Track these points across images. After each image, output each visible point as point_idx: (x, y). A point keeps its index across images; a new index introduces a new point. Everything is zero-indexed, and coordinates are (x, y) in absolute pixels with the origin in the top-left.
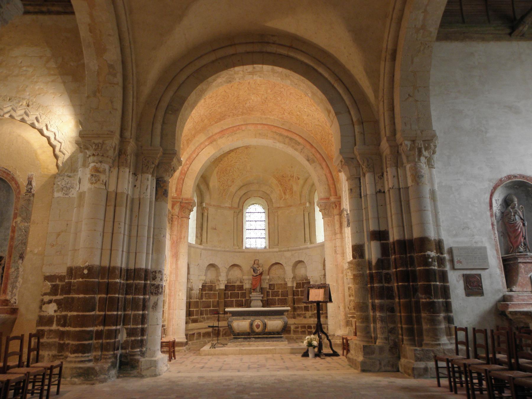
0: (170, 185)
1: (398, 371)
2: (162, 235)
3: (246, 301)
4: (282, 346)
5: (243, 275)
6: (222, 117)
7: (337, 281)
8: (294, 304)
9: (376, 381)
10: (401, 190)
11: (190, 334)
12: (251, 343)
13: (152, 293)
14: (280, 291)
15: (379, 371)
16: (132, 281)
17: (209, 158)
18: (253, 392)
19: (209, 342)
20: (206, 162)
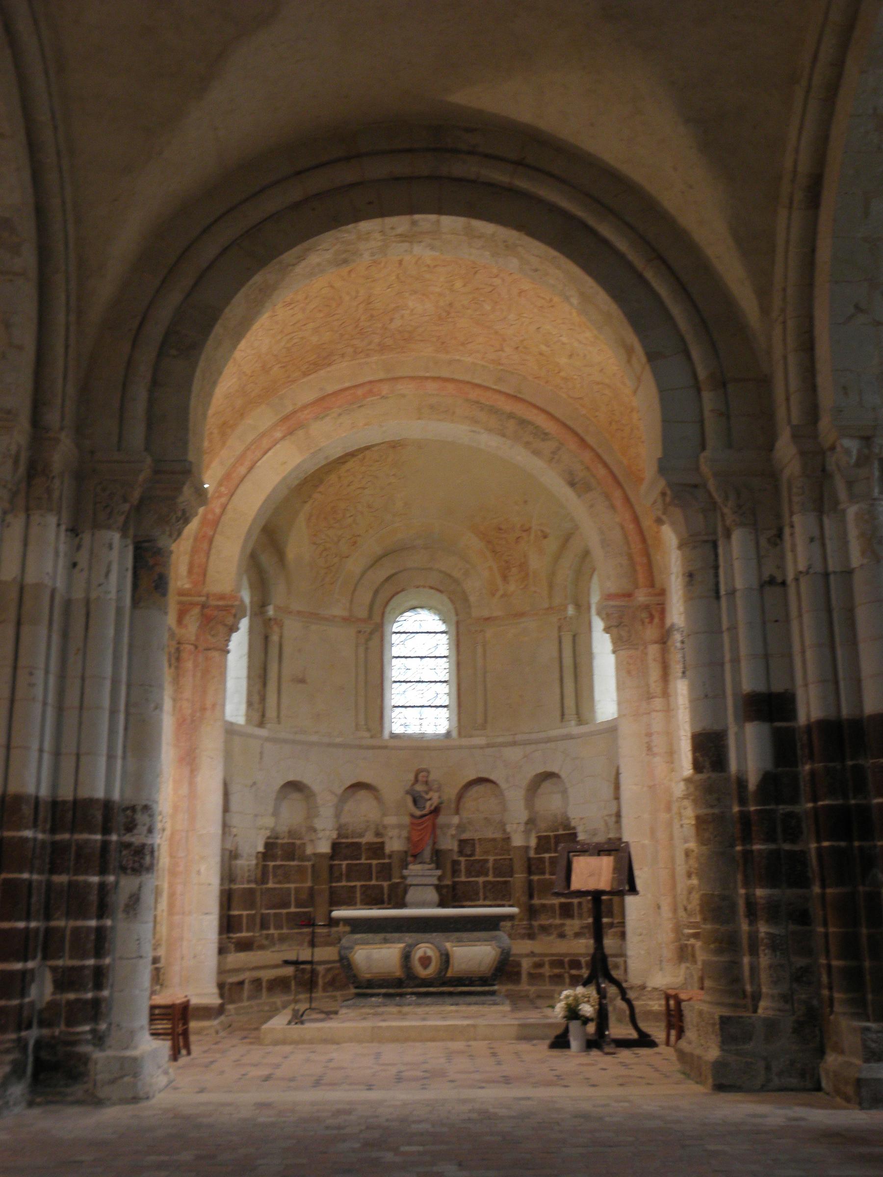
0: (174, 557)
1: (818, 1088)
2: (152, 705)
3: (393, 887)
4: (494, 1016)
5: (384, 815)
6: (322, 360)
7: (653, 832)
8: (531, 897)
9: (755, 1116)
10: (832, 578)
11: (232, 984)
12: (406, 1009)
13: (123, 869)
14: (491, 858)
15: (764, 1088)
16: (67, 836)
17: (285, 479)
18: (409, 1144)
19: (284, 1007)
20: (274, 490)
